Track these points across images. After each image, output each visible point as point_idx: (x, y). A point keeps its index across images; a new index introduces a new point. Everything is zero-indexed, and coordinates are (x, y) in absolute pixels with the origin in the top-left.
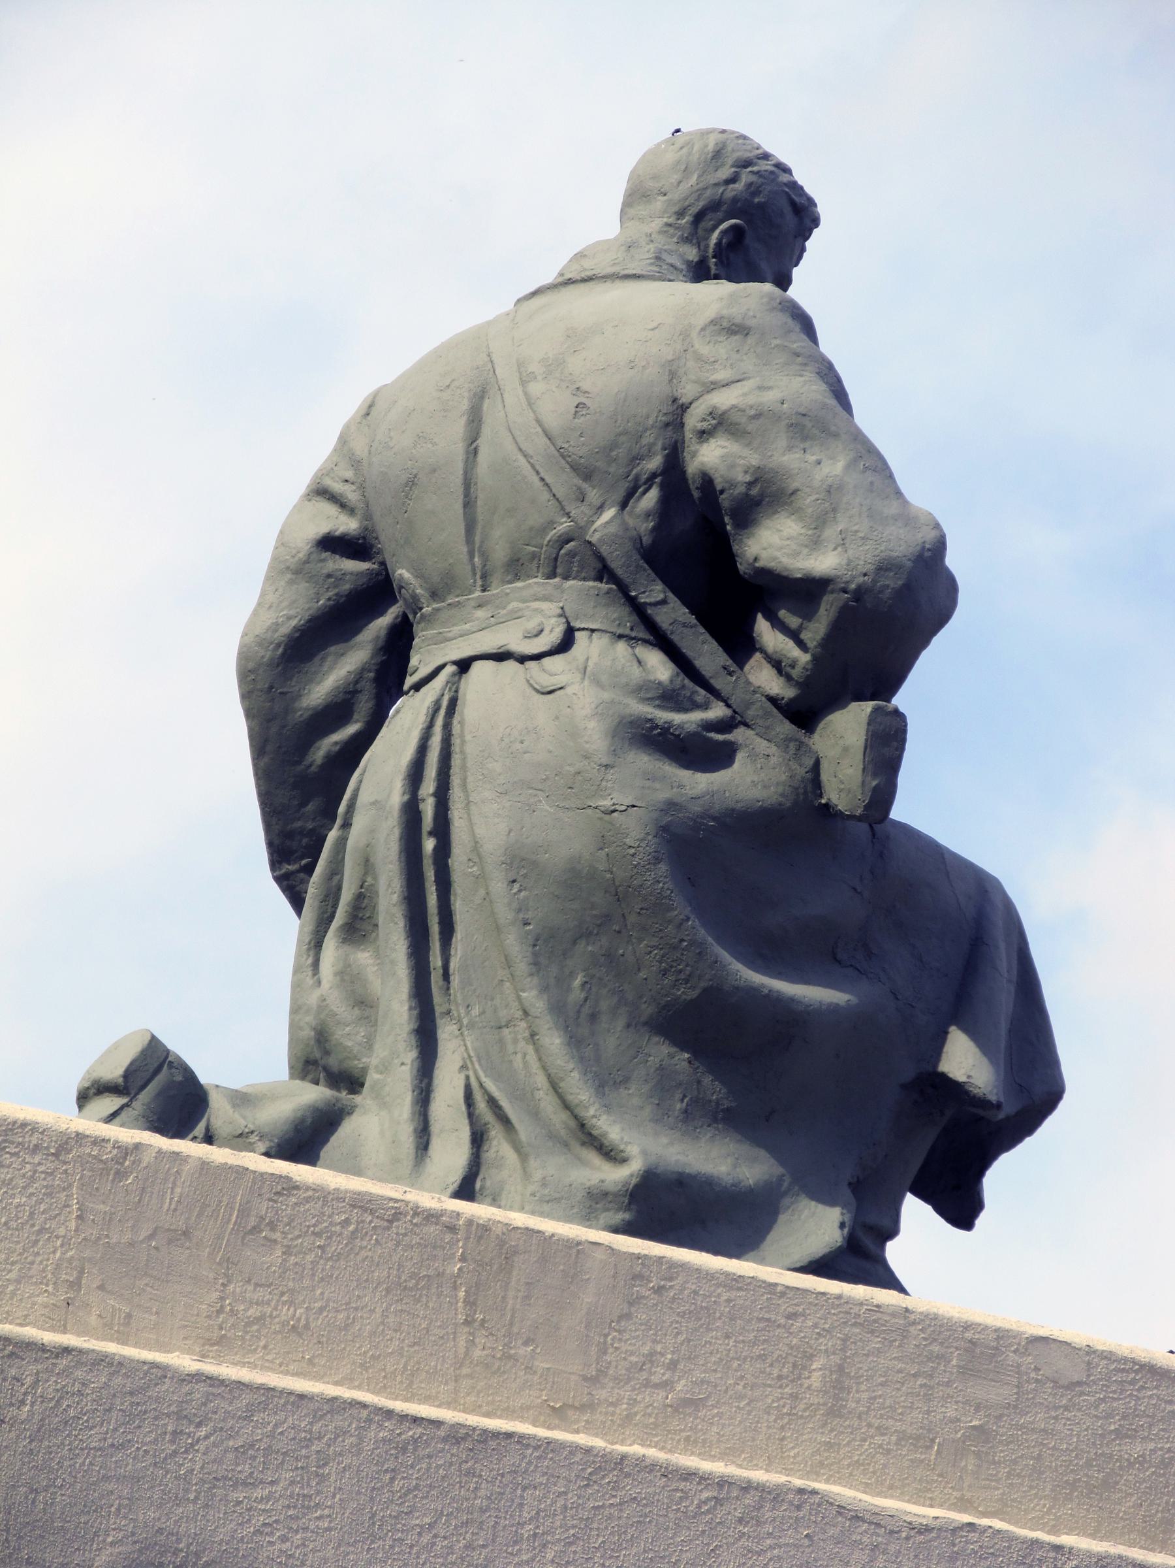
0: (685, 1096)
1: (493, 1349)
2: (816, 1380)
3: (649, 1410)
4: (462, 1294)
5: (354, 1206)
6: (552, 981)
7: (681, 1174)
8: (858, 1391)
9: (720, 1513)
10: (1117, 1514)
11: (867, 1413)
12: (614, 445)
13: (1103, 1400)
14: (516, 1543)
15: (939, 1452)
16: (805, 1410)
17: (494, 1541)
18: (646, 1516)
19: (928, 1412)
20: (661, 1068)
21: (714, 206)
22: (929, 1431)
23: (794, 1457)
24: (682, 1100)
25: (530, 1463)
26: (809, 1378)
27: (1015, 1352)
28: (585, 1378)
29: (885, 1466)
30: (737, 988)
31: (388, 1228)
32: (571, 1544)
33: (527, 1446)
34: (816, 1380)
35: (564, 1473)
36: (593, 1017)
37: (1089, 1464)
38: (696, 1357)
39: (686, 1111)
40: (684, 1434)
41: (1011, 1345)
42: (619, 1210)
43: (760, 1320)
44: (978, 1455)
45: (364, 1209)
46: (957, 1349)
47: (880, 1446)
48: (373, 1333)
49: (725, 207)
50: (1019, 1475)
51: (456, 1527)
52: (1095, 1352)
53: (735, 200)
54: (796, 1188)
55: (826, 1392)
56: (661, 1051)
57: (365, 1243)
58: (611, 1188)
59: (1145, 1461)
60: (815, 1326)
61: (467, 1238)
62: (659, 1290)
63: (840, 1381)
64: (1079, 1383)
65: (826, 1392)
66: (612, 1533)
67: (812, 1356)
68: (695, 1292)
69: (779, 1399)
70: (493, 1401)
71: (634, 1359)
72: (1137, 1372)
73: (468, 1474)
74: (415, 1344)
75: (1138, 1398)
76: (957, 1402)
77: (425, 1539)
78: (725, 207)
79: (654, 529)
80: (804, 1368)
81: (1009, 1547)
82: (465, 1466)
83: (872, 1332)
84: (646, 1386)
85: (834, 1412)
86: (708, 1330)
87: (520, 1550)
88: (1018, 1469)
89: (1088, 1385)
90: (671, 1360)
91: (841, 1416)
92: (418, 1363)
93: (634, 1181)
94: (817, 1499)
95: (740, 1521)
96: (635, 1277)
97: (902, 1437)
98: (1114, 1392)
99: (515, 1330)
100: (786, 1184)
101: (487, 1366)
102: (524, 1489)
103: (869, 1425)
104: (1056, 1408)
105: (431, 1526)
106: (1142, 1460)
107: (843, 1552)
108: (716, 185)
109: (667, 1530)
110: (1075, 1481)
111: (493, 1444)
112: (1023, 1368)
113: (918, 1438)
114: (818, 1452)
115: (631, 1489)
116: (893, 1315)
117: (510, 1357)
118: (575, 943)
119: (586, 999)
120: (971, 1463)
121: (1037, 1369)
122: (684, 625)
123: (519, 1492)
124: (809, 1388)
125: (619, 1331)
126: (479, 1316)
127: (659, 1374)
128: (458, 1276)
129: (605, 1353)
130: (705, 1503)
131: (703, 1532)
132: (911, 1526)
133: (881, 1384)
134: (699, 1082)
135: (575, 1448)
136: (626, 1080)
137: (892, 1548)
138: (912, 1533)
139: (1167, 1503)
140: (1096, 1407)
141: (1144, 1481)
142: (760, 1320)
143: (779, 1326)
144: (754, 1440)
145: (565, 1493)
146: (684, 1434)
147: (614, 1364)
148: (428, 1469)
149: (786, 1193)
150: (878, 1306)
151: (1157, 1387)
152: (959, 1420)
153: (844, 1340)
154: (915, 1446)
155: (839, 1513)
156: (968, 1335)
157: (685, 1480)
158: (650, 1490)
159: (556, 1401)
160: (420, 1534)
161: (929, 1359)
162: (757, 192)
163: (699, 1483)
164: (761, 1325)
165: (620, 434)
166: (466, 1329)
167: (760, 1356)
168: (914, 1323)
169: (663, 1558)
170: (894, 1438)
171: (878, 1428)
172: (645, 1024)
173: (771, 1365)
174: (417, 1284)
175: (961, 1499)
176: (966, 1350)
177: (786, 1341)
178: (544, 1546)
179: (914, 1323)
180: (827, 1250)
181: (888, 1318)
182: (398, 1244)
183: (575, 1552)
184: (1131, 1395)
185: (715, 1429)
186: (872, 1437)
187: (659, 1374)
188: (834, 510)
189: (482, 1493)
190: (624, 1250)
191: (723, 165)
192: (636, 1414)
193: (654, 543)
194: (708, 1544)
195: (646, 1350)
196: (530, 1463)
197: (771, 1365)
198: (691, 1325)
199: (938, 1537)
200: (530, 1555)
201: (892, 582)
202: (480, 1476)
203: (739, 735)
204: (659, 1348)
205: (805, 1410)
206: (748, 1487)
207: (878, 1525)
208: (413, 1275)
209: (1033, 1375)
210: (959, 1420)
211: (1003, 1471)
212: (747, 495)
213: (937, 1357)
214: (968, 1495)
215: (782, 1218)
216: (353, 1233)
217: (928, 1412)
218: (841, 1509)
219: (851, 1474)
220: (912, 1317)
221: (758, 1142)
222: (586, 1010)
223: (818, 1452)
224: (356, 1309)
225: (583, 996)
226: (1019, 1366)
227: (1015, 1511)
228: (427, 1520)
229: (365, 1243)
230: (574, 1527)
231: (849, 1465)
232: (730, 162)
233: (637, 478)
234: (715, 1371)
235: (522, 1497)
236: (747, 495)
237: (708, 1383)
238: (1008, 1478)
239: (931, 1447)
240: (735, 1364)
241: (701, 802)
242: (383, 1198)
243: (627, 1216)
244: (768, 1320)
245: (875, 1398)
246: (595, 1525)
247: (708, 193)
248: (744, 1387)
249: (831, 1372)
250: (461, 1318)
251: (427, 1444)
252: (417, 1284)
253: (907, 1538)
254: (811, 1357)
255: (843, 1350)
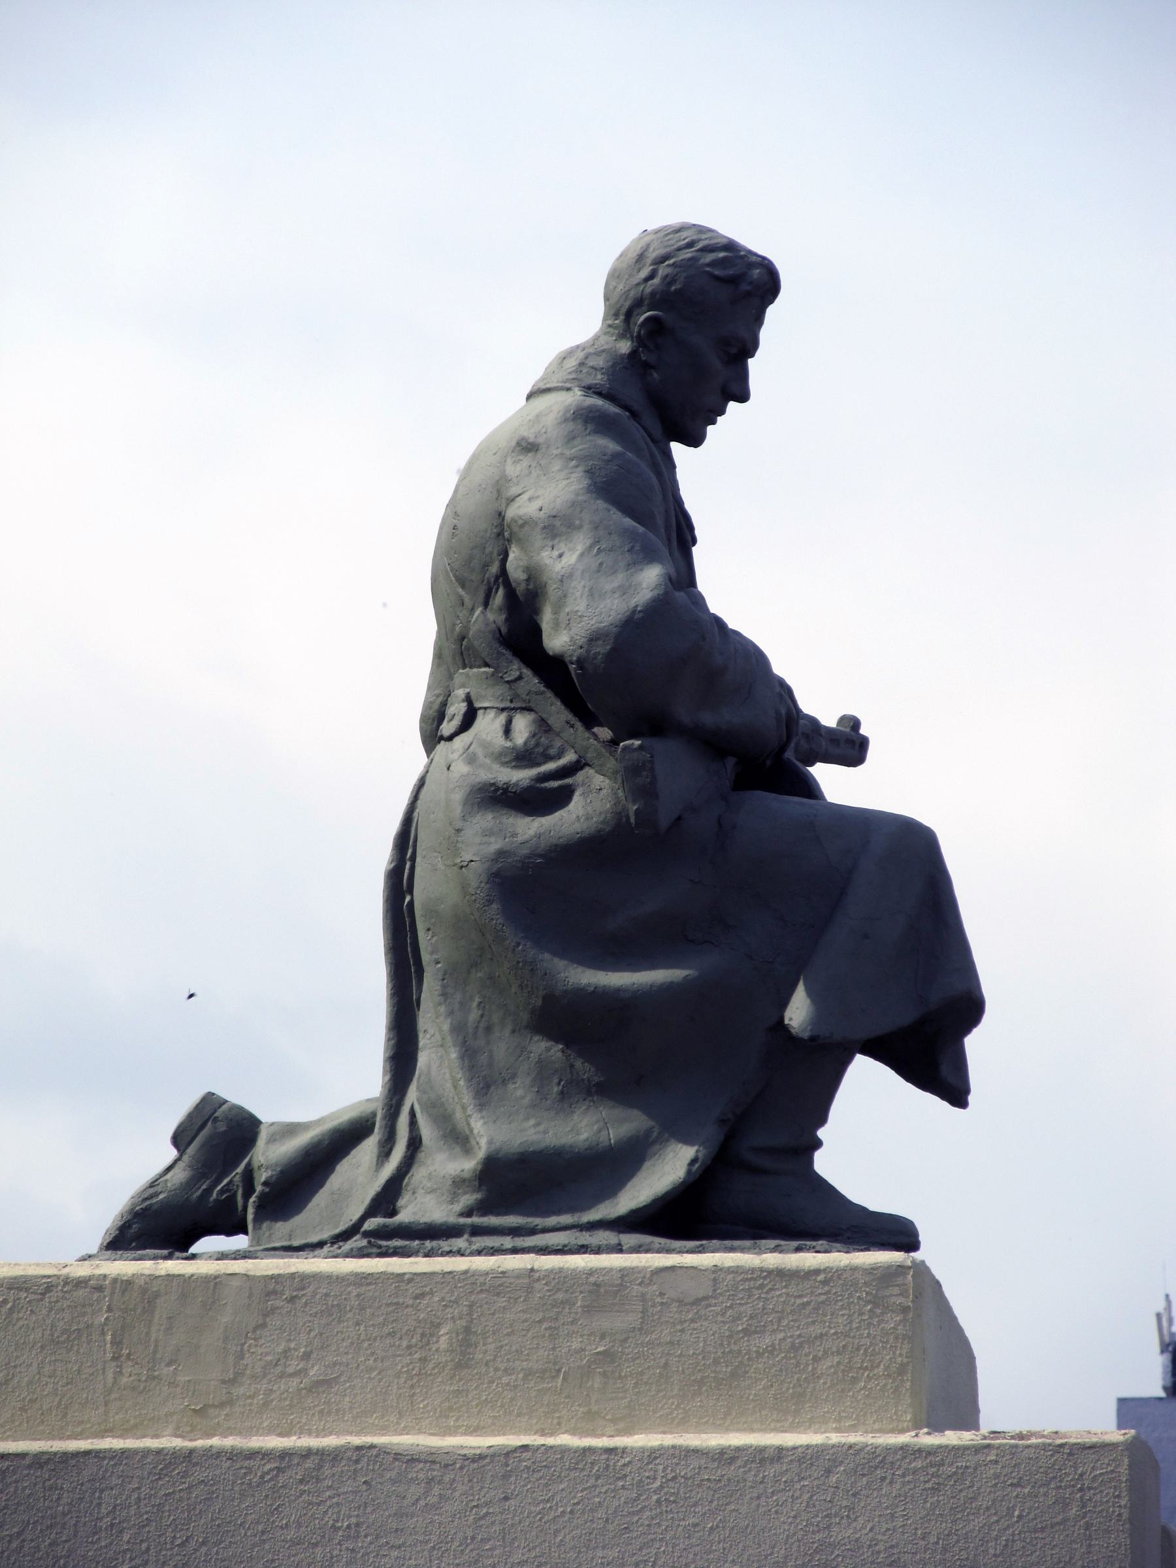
0: (561, 1080)
1: (139, 1374)
2: (443, 1343)
3: (285, 1396)
4: (109, 1338)
5: (10, 1289)
6: (457, 1006)
7: (522, 1153)
8: (484, 1345)
9: (281, 1480)
10: (748, 1398)
11: (494, 1360)
12: (471, 558)
13: (731, 1307)
14: (95, 1533)
15: (564, 1379)
16: (433, 1369)
17: (75, 1535)
18: (213, 1492)
19: (554, 1349)
20: (540, 1061)
21: (638, 304)
22: (555, 1363)
23: (424, 1407)
24: (559, 1084)
25: (106, 1471)
26: (437, 1342)
27: (640, 1284)
28: (223, 1382)
29: (512, 1399)
30: (566, 992)
31: (42, 1300)
32: (144, 1526)
33: (104, 1458)
34: (443, 1343)
35: (138, 1473)
36: (489, 1029)
37: (716, 1362)
38: (329, 1346)
39: (562, 1092)
40: (318, 1408)
41: (636, 1279)
42: (474, 1191)
43: (388, 1305)
44: (604, 1374)
45: (20, 1289)
46: (581, 1292)
47: (508, 1384)
48: (30, 1383)
49: (646, 302)
50: (646, 1383)
51: (41, 1531)
52: (721, 1270)
53: (653, 294)
54: (666, 1135)
55: (452, 1351)
56: (542, 1047)
57: (21, 1315)
58: (466, 1175)
59: (774, 1348)
60: (443, 1299)
61: (113, 1293)
62: (292, 1300)
63: (466, 1340)
64: (705, 1298)
65: (452, 1351)
66: (183, 1512)
67: (439, 1324)
68: (327, 1295)
69: (408, 1365)
70: (140, 1414)
71: (269, 1358)
72: (765, 1278)
73: (51, 1488)
74: (68, 1384)
75: (767, 1299)
76: (582, 1336)
77: (14, 1545)
78: (646, 302)
79: (507, 620)
80: (432, 1335)
81: (562, 1458)
82: (48, 1484)
83: (498, 1294)
84: (281, 1377)
85: (459, 1366)
86: (339, 1322)
87: (99, 1539)
88: (645, 1378)
89: (715, 1298)
90: (304, 1353)
91: (468, 1367)
92: (71, 1398)
93: (479, 1167)
94: (374, 1452)
95: (301, 1481)
96: (268, 1294)
97: (529, 1373)
98: (742, 1299)
99: (158, 1356)
100: (655, 1134)
101: (134, 1389)
102: (102, 1491)
103: (497, 1369)
104: (681, 1322)
105: (19, 1534)
106: (771, 1350)
107: (400, 1489)
108: (638, 285)
109: (233, 1500)
110: (703, 1378)
111: (73, 1462)
112: (648, 1296)
113: (544, 1371)
114: (448, 1399)
115: (198, 1474)
116: (518, 1277)
117: (154, 1378)
118: (469, 972)
119: (482, 1016)
120: (597, 1382)
121: (662, 1294)
122: (537, 693)
123: (97, 1495)
124: (437, 1350)
125: (255, 1339)
126: (125, 1352)
127: (294, 1365)
128: (105, 1324)
129: (243, 1358)
130: (268, 1473)
131: (267, 1496)
132: (465, 1457)
133: (508, 1334)
134: (572, 1066)
135: (147, 1452)
136: (514, 1076)
137: (447, 1479)
138: (466, 1463)
139: (798, 1380)
140: (723, 1315)
141: (774, 1365)
142: (388, 1305)
143: (407, 1306)
144: (385, 1400)
145: (138, 1488)
146: (318, 1408)
147: (250, 1366)
148: (15, 1491)
149: (654, 1142)
150: (502, 1273)
151: (786, 1287)
152: (584, 1350)
153: (470, 1306)
154: (542, 1378)
155: (395, 1459)
156: (592, 1280)
157: (250, 1458)
158: (217, 1472)
159: (196, 1404)
160: (10, 1542)
161: (554, 1306)
162: (670, 284)
163: (262, 1459)
164: (390, 1309)
165: (473, 549)
166: (114, 1364)
167: (389, 1334)
168: (539, 1280)
169: (230, 1522)
170: (521, 1376)
171: (506, 1370)
172: (527, 1027)
173: (401, 1338)
174: (69, 1337)
175: (589, 1412)
176: (590, 1292)
177: (414, 1317)
178: (121, 1532)
179: (539, 1280)
180: (670, 1187)
181: (512, 1280)
182: (51, 1309)
183: (149, 1532)
184: (759, 1298)
185: (347, 1399)
186: (500, 1378)
187: (294, 1365)
188: (565, 596)
189: (64, 1501)
190: (259, 1274)
191: (644, 266)
192: (272, 1401)
193: (509, 630)
194: (271, 1505)
195: (280, 1349)
196: (106, 1471)
197: (401, 1338)
198: (324, 1321)
199: (492, 1461)
200: (108, 1541)
201: (602, 648)
202: (62, 1488)
203: (580, 776)
204: (292, 1345)
205: (433, 1369)
206: (308, 1453)
207: (433, 1462)
208: (64, 1331)
209: (659, 1300)
210: (584, 1350)
211: (630, 1383)
212: (528, 589)
213: (562, 1302)
214: (594, 1408)
215: (647, 1164)
216: (10, 1309)
217: (554, 1349)
218: (397, 1456)
219: (479, 1412)
220: (537, 1275)
221: (630, 1104)
222: (482, 1025)
223: (448, 1399)
224: (15, 1367)
225: (480, 1012)
226: (643, 1295)
227: (643, 1413)
228: (15, 1530)
229: (21, 1315)
230: (147, 1513)
231: (477, 1405)
232: (649, 261)
233: (489, 582)
234: (347, 1353)
235: (100, 1498)
236: (528, 589)
237: (340, 1364)
238: (634, 1387)
239: (557, 1376)
240: (366, 1344)
241: (528, 845)
242: (36, 1277)
243: (478, 1196)
244: (397, 1304)
245: (502, 1347)
246: (167, 1508)
247: (632, 292)
248: (375, 1360)
249: (457, 1334)
250: (109, 1356)
251: (14, 1472)
252: (69, 1337)
253: (462, 1468)
254: (438, 1326)
255: (470, 1314)
